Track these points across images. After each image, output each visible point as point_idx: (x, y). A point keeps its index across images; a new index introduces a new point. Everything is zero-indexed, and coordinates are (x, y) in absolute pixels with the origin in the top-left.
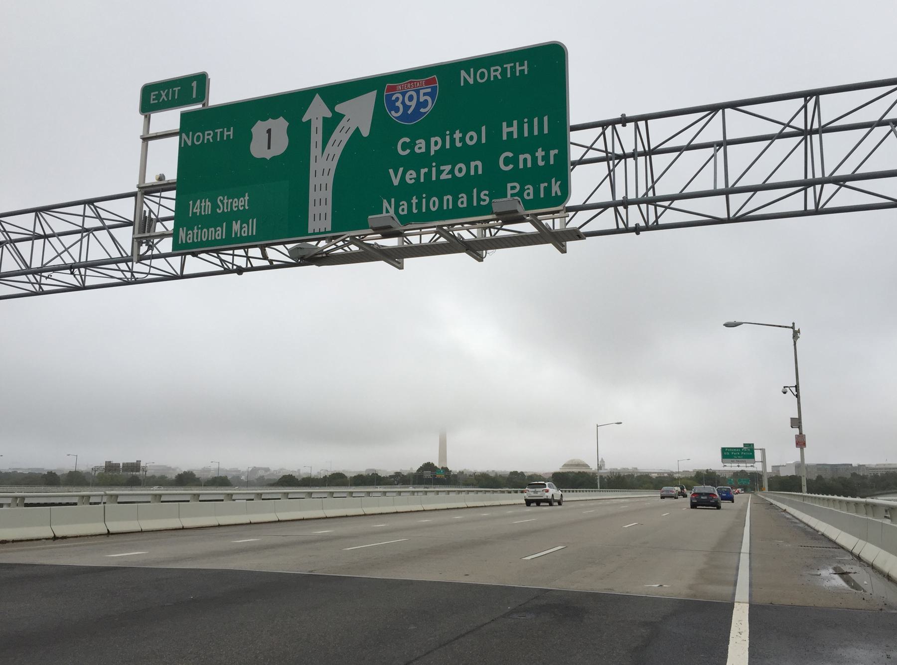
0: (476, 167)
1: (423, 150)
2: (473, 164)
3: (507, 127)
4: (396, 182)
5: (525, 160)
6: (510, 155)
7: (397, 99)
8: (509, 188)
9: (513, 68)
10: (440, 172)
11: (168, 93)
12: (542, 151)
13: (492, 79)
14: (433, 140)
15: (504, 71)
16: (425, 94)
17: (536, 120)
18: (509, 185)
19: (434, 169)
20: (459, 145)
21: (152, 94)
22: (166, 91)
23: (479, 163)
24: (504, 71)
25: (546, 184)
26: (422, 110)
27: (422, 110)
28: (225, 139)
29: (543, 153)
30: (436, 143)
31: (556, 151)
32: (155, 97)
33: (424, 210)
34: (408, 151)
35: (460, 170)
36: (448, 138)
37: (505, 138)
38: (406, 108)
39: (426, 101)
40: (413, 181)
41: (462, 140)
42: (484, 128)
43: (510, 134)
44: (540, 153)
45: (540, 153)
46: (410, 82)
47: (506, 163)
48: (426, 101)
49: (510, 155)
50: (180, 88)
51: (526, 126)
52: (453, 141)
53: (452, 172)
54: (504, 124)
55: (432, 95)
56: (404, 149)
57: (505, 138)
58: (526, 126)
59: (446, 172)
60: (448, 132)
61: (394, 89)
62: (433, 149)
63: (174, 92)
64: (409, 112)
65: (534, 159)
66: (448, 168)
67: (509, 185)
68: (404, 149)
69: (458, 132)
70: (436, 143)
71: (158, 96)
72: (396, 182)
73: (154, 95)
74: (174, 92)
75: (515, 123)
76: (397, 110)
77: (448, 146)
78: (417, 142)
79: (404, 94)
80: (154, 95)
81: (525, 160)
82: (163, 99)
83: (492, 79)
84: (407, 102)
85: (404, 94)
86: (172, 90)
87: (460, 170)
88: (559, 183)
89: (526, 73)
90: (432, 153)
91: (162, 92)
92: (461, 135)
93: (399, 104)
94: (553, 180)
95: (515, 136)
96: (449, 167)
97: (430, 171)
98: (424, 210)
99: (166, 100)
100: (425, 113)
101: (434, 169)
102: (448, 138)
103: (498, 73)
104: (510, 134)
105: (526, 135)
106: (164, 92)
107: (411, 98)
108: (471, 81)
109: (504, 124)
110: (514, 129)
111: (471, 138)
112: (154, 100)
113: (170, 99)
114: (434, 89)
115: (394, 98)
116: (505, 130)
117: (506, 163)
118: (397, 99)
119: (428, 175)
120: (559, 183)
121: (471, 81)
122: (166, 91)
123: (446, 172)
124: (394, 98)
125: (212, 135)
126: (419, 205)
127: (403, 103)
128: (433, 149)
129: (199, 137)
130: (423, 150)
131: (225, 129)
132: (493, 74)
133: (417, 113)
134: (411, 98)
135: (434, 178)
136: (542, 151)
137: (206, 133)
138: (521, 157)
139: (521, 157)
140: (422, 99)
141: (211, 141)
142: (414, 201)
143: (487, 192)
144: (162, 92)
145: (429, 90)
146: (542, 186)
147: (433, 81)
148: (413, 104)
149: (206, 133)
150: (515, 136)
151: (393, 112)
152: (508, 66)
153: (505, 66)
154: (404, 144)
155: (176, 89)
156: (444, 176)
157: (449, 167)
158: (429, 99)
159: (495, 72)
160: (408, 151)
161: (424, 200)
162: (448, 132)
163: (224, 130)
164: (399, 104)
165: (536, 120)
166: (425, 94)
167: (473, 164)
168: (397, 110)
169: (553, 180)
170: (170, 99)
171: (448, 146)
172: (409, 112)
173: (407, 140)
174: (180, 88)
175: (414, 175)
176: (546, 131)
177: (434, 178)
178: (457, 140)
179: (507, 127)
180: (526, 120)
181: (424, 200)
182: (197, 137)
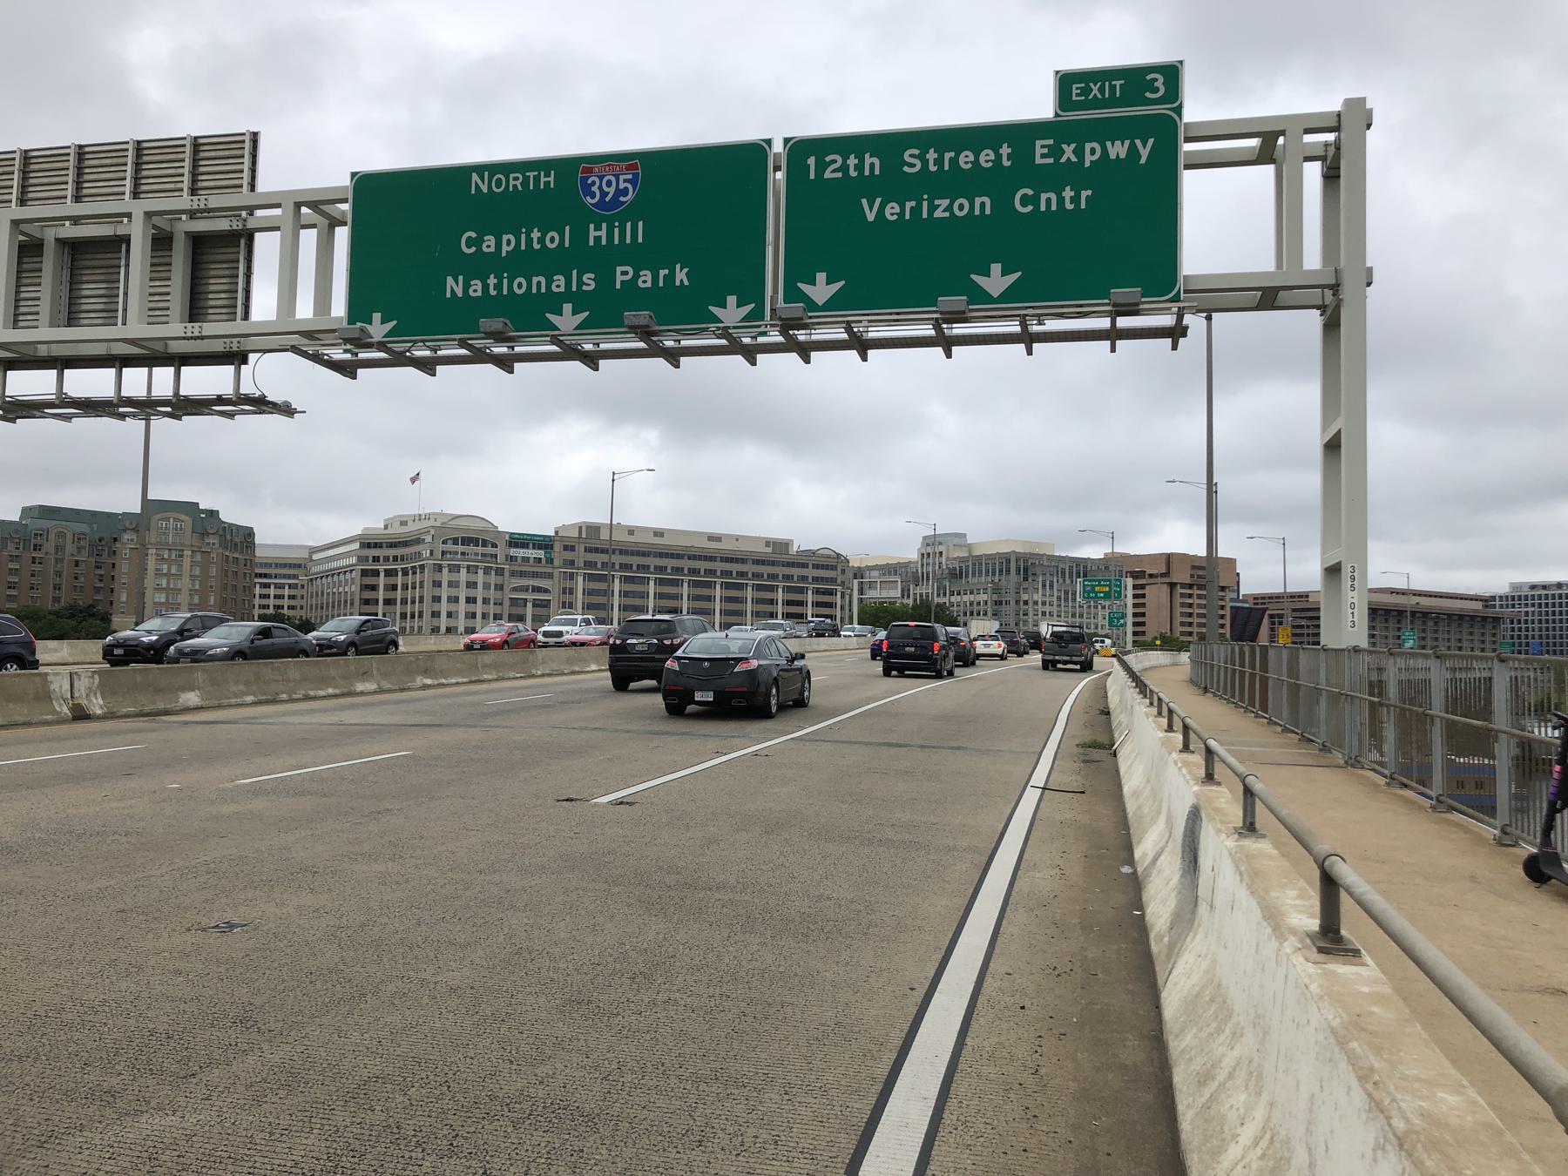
0: (983, 205)
1: (492, 249)
2: (978, 201)
3: (595, 230)
4: (871, 217)
5: (1049, 201)
6: (1030, 192)
7: (594, 183)
8: (618, 273)
9: (537, 179)
10: (932, 208)
11: (1103, 86)
12: (1071, 190)
13: (511, 189)
14: (505, 238)
15: (526, 179)
16: (625, 181)
17: (629, 225)
18: (619, 269)
19: (925, 204)
20: (537, 246)
21: (1074, 86)
22: (1099, 84)
23: (987, 200)
24: (526, 179)
25: (666, 271)
26: (622, 199)
27: (622, 199)
28: (542, 187)
29: (1073, 194)
30: (1093, 151)
31: (1089, 192)
32: (1079, 91)
33: (505, 292)
34: (474, 249)
35: (961, 207)
36: (523, 236)
37: (591, 243)
38: (605, 194)
39: (626, 188)
40: (895, 217)
41: (541, 240)
42: (567, 228)
43: (597, 239)
44: (1068, 193)
45: (1068, 193)
46: (609, 165)
47: (1024, 203)
48: (626, 188)
49: (1030, 192)
50: (1123, 82)
51: (616, 230)
52: (529, 241)
53: (949, 208)
54: (592, 226)
55: (633, 182)
56: (469, 247)
57: (591, 243)
58: (616, 230)
59: (941, 208)
60: (925, 197)
61: (590, 170)
62: (505, 249)
63: (1113, 88)
64: (607, 199)
65: (486, 287)
66: (945, 203)
67: (619, 269)
68: (1024, 205)
69: (536, 230)
70: (1093, 151)
71: (1086, 91)
72: (871, 217)
73: (1077, 88)
74: (1113, 88)
75: (604, 225)
76: (593, 196)
77: (523, 248)
78: (486, 238)
79: (601, 178)
80: (1077, 88)
81: (1049, 201)
82: (1095, 94)
83: (511, 189)
84: (606, 189)
85: (601, 178)
86: (1110, 85)
87: (961, 207)
88: (686, 270)
89: (552, 186)
90: (504, 254)
91: (1091, 85)
92: (539, 235)
93: (595, 189)
94: (678, 266)
95: (604, 242)
96: (947, 202)
97: (919, 206)
98: (505, 292)
99: (1100, 97)
100: (625, 202)
101: (925, 204)
102: (523, 236)
103: (518, 183)
104: (597, 239)
105: (628, 241)
106: (1095, 85)
107: (609, 184)
108: (485, 189)
109: (592, 226)
110: (603, 233)
111: (552, 240)
112: (1077, 95)
113: (1107, 96)
114: (636, 176)
115: (589, 181)
116: (593, 233)
117: (1024, 203)
118: (594, 183)
119: (916, 211)
120: (686, 270)
121: (485, 189)
122: (1099, 84)
123: (941, 208)
124: (589, 181)
125: (521, 180)
126: (498, 287)
127: (600, 188)
128: (505, 249)
129: (499, 180)
130: (492, 249)
131: (542, 173)
132: (512, 183)
133: (615, 202)
134: (609, 184)
135: (925, 216)
136: (1071, 190)
137: (512, 176)
138: (1044, 197)
139: (1044, 197)
140: (622, 186)
141: (520, 188)
142: (492, 281)
143: (592, 276)
144: (1091, 85)
145: (630, 177)
146: (663, 272)
147: (634, 167)
148: (612, 190)
149: (512, 176)
150: (604, 242)
151: (588, 198)
152: (531, 174)
153: (527, 174)
154: (1024, 197)
155: (1118, 83)
156: (938, 214)
157: (947, 202)
158: (629, 186)
159: (515, 181)
160: (1030, 208)
161: (505, 281)
162: (524, 230)
163: (540, 174)
164: (595, 189)
165: (629, 225)
166: (625, 181)
167: (978, 201)
168: (593, 196)
169: (678, 266)
170: (1107, 96)
171: (523, 248)
172: (607, 199)
173: (473, 235)
174: (1123, 82)
175: (897, 210)
176: (640, 240)
177: (925, 216)
178: (1067, 201)
179: (595, 230)
180: (617, 224)
181: (505, 281)
182: (501, 184)
